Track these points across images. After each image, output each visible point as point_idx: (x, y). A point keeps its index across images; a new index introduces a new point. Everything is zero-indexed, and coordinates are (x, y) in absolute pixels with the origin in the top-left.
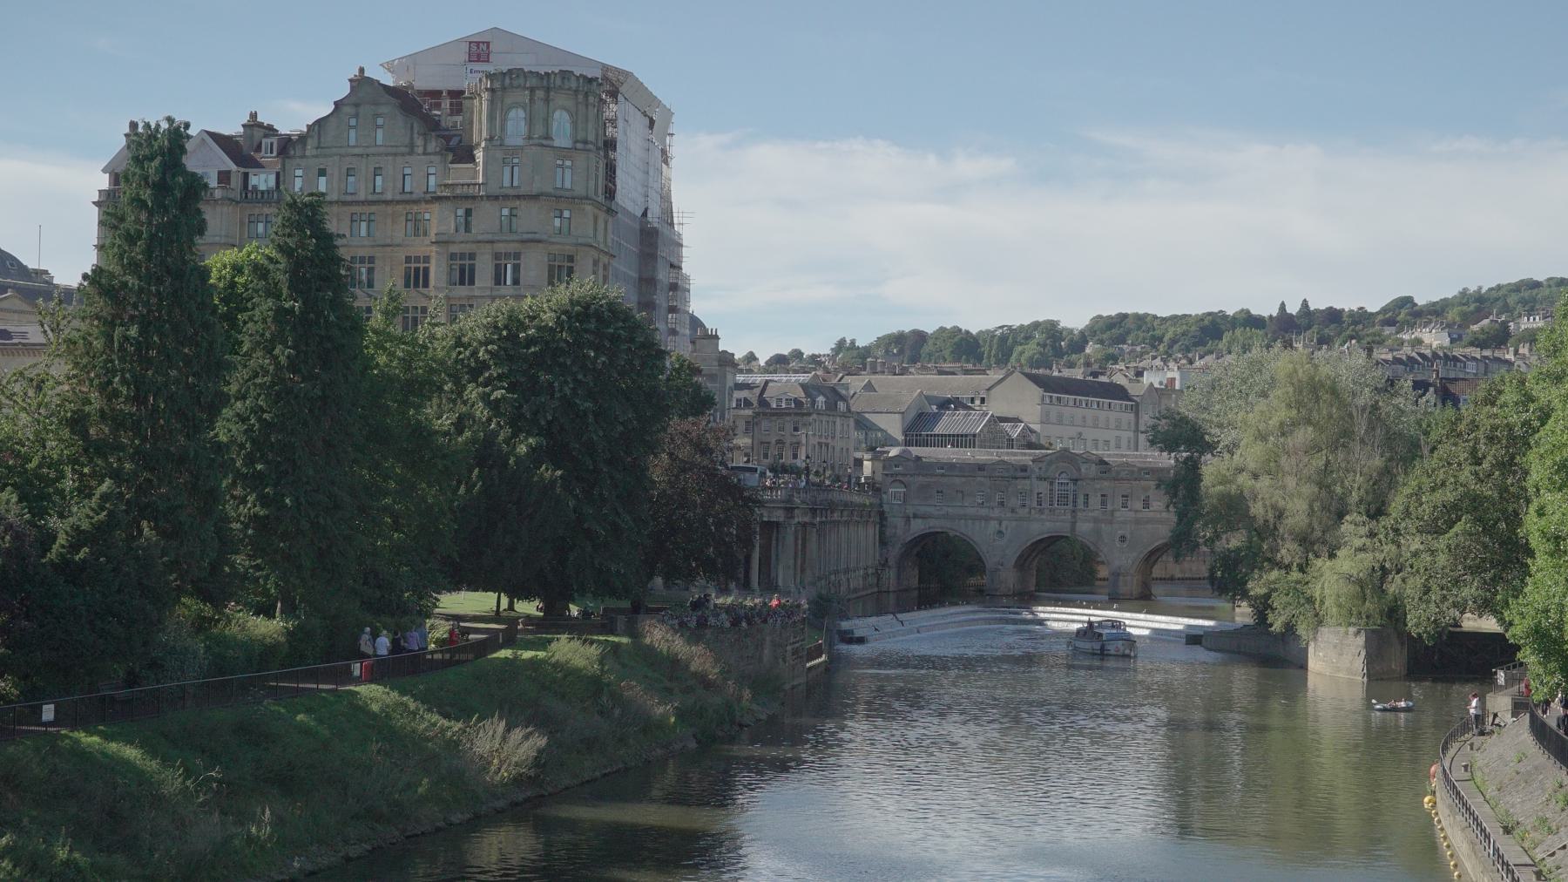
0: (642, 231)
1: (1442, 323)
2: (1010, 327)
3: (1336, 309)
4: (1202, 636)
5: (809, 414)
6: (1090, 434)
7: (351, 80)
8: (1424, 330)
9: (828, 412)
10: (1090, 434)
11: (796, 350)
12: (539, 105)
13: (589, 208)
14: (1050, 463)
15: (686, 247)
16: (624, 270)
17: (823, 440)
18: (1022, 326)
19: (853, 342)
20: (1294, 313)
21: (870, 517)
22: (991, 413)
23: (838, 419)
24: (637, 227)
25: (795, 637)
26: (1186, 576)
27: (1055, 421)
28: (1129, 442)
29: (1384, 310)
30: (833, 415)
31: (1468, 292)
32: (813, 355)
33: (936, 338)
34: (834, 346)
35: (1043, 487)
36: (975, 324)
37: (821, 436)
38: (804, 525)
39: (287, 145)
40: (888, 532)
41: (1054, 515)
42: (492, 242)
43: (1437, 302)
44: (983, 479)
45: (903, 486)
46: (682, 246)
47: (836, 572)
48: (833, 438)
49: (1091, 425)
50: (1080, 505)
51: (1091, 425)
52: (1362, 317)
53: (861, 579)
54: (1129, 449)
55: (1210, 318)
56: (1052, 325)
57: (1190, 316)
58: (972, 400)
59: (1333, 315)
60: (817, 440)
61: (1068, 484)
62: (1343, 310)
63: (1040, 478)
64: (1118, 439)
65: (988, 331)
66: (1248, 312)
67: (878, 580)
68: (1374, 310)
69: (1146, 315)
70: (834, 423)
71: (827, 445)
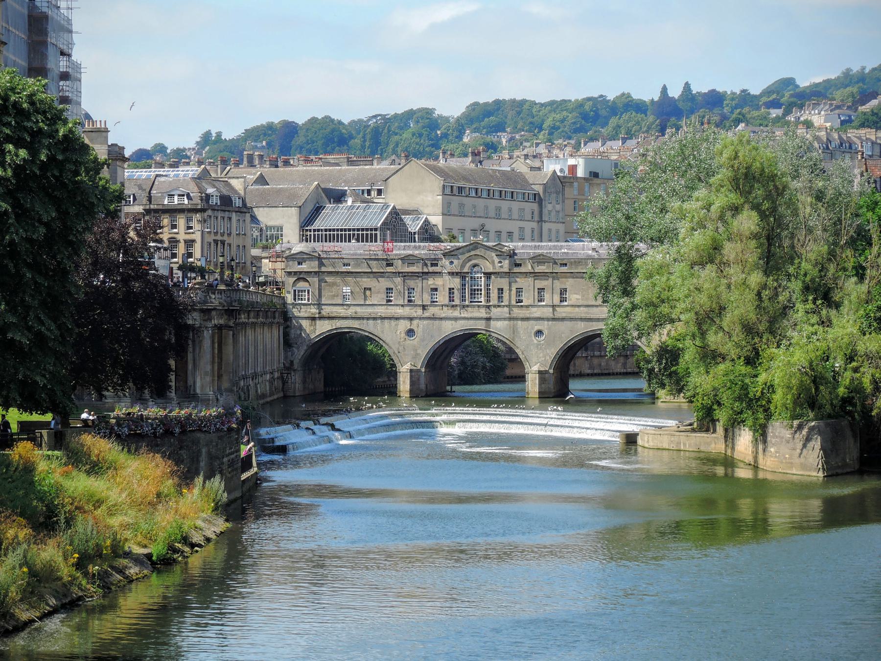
0: (30, 16)
1: (831, 105)
2: (383, 117)
3: (719, 93)
6: (492, 225)
8: (813, 112)
9: (223, 208)
10: (492, 225)
11: (159, 145)
15: (77, 33)
16: (14, 58)
17: (219, 238)
18: (396, 116)
19: (219, 135)
20: (676, 97)
21: (274, 318)
22: (392, 205)
23: (234, 216)
24: (26, 12)
25: (231, 448)
26: (595, 371)
27: (456, 213)
29: (767, 92)
30: (229, 211)
31: (851, 73)
32: (178, 149)
33: (307, 130)
34: (199, 140)
35: (456, 282)
36: (729, 86)
37: (216, 233)
38: (220, 328)
40: (293, 333)
43: (820, 83)
46: (71, 32)
47: (245, 378)
48: (229, 235)
49: (494, 216)
50: (494, 301)
51: (494, 216)
52: (745, 98)
53: (267, 384)
54: (533, 240)
55: (591, 103)
56: (428, 112)
57: (570, 101)
58: (369, 192)
59: (714, 99)
60: (213, 237)
62: (726, 92)
63: (451, 274)
64: (522, 229)
65: (360, 121)
66: (629, 96)
67: (284, 384)
68: (758, 93)
69: (524, 102)
70: (230, 219)
71: (223, 242)
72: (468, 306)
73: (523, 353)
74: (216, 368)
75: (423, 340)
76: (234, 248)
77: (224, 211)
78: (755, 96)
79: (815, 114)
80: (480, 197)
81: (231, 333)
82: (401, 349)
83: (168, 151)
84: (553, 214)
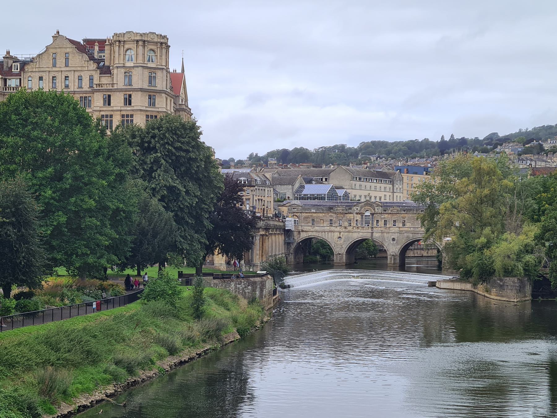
4: (436, 282)
5: (254, 186)
7: (53, 37)
12: (141, 48)
13: (163, 95)
14: (361, 208)
17: (260, 198)
19: (256, 155)
20: (448, 140)
26: (415, 255)
28: (390, 196)
34: (248, 156)
35: (358, 217)
38: (262, 235)
39: (24, 64)
41: (363, 229)
42: (121, 111)
44: (332, 214)
45: (297, 218)
48: (264, 197)
50: (375, 225)
59: (463, 142)
61: (369, 215)
63: (357, 213)
70: (264, 190)
71: (262, 200)
72: (364, 227)
73: (386, 248)
74: (261, 252)
75: (345, 241)
76: (266, 202)
77: (263, 187)
78: (481, 140)
79: (507, 148)
80: (368, 182)
81: (267, 237)
82: (336, 245)
83: (236, 161)
84: (398, 189)
